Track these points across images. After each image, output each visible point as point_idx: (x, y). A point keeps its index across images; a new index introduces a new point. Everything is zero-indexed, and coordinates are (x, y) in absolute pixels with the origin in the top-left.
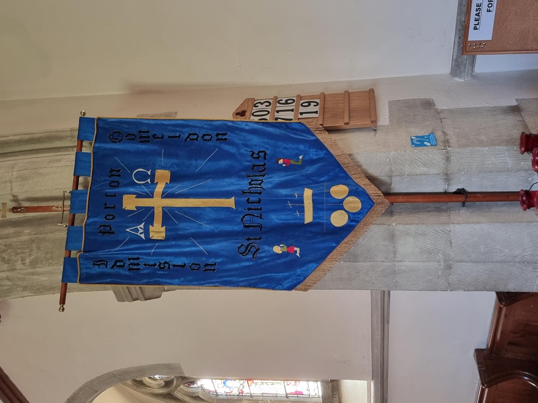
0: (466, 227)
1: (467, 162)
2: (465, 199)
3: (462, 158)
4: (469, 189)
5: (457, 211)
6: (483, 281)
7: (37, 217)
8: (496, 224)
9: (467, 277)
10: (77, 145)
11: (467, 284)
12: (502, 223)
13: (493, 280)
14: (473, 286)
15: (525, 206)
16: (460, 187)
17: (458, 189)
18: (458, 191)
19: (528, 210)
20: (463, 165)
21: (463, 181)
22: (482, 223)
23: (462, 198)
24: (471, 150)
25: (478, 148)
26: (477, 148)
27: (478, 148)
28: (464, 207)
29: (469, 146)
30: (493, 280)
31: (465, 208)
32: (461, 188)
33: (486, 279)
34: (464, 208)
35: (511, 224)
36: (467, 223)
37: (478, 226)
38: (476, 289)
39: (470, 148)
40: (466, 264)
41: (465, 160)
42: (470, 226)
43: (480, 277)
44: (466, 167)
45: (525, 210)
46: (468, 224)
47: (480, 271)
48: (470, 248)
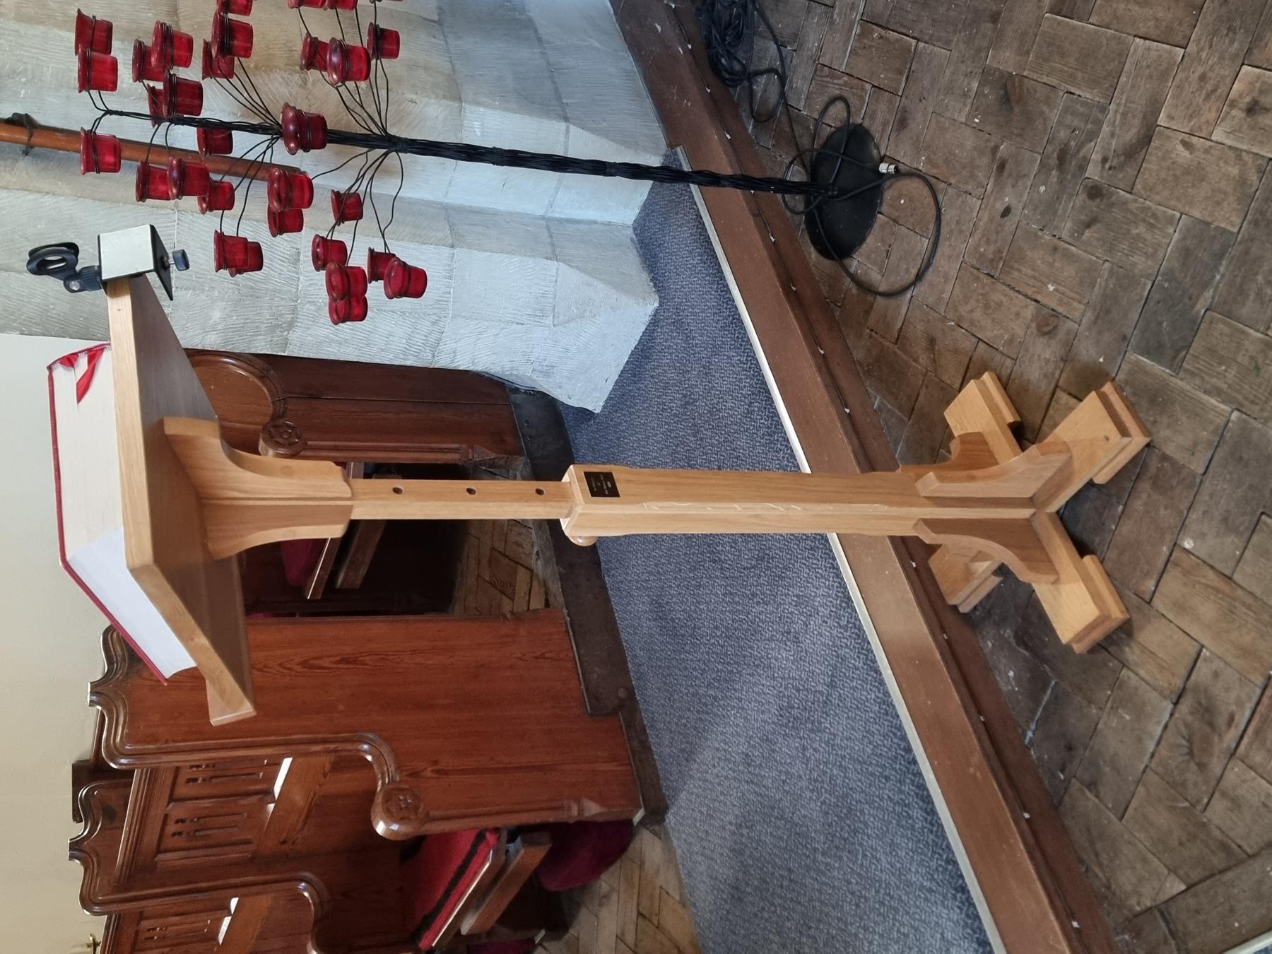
0: (22, 198)
1: (33, 58)
2: (27, 138)
3: (23, 46)
4: (40, 119)
5: (9, 162)
6: (59, 315)
7: (1134, 141)
8: (89, 202)
9: (24, 306)
10: (196, 129)
11: (24, 320)
12: (99, 200)
13: (81, 317)
14: (39, 325)
15: (204, 205)
16: (21, 111)
17: (15, 114)
18: (16, 118)
19: (208, 212)
20: (24, 63)
21: (24, 98)
22: (59, 195)
23: (22, 136)
24: (43, 33)
25: (61, 33)
26: (56, 31)
27: (61, 33)
28: (27, 155)
29: (41, 23)
30: (81, 317)
31: (30, 158)
32: (23, 113)
33: (65, 313)
34: (27, 157)
35: (119, 206)
36: (25, 190)
37: (48, 201)
38: (46, 333)
39: (41, 28)
40: (19, 276)
41: (28, 51)
42: (31, 197)
43: (51, 307)
44: (30, 67)
45: (203, 212)
46: (27, 192)
47: (49, 293)
48: (28, 243)
